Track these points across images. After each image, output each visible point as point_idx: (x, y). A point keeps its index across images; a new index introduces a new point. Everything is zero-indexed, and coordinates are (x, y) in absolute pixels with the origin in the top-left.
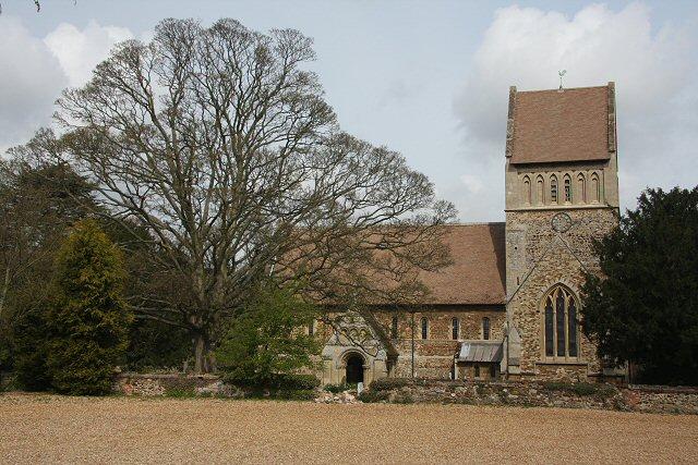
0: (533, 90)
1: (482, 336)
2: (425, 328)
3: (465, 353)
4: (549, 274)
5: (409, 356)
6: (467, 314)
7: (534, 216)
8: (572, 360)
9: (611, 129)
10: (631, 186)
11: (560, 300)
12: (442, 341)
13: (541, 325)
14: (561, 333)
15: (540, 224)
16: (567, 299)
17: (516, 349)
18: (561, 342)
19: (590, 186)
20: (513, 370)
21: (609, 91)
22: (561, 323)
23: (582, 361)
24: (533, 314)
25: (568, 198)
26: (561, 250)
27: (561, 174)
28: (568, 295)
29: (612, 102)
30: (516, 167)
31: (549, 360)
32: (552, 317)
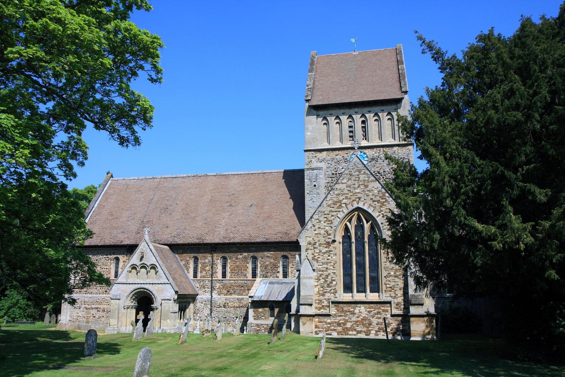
1: (281, 275)
2: (224, 267)
4: (346, 198)
5: (208, 296)
6: (266, 253)
7: (333, 154)
8: (373, 297)
11: (360, 227)
13: (339, 258)
14: (361, 266)
15: (338, 162)
16: (367, 226)
17: (310, 288)
18: (361, 276)
19: (386, 125)
20: (304, 310)
22: (360, 253)
23: (385, 297)
24: (328, 244)
25: (375, 289)
26: (360, 171)
31: (347, 297)
32: (350, 246)
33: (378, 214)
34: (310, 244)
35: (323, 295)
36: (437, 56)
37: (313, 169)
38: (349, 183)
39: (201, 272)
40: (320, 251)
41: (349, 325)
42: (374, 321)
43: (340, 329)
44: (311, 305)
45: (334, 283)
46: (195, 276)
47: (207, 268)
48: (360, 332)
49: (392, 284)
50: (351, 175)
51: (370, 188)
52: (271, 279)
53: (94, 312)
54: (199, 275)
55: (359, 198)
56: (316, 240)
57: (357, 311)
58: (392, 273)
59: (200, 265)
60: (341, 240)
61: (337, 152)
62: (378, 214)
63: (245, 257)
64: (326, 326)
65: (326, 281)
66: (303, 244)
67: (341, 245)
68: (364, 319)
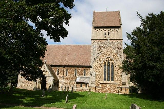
0: (99, 12)
1: (83, 75)
2: (67, 72)
3: (78, 80)
4: (105, 54)
5: (62, 80)
9: (120, 20)
10: (131, 24)
11: (109, 63)
12: (72, 76)
13: (102, 71)
14: (109, 74)
15: (101, 44)
16: (111, 63)
18: (108, 76)
21: (119, 12)
22: (109, 70)
24: (100, 67)
25: (112, 80)
26: (109, 47)
27: (107, 30)
28: (111, 61)
29: (120, 14)
30: (95, 28)
31: (105, 82)
33: (114, 59)
34: (95, 67)
35: (98, 81)
36: (141, 18)
37: (94, 45)
38: (106, 50)
39: (60, 73)
40: (97, 69)
41: (105, 90)
42: (112, 89)
43: (102, 91)
44: (95, 84)
45: (101, 78)
46: (58, 75)
47: (62, 72)
48: (108, 92)
49: (117, 79)
50: (107, 48)
51: (112, 52)
52: (81, 76)
53: (28, 84)
54: (59, 74)
55: (109, 55)
56: (96, 66)
57: (107, 86)
58: (118, 76)
59: (59, 72)
60: (103, 66)
61: (101, 41)
62: (114, 59)
63: (73, 70)
64: (98, 90)
65: (99, 78)
66: (93, 66)
67: (103, 68)
68: (109, 88)
